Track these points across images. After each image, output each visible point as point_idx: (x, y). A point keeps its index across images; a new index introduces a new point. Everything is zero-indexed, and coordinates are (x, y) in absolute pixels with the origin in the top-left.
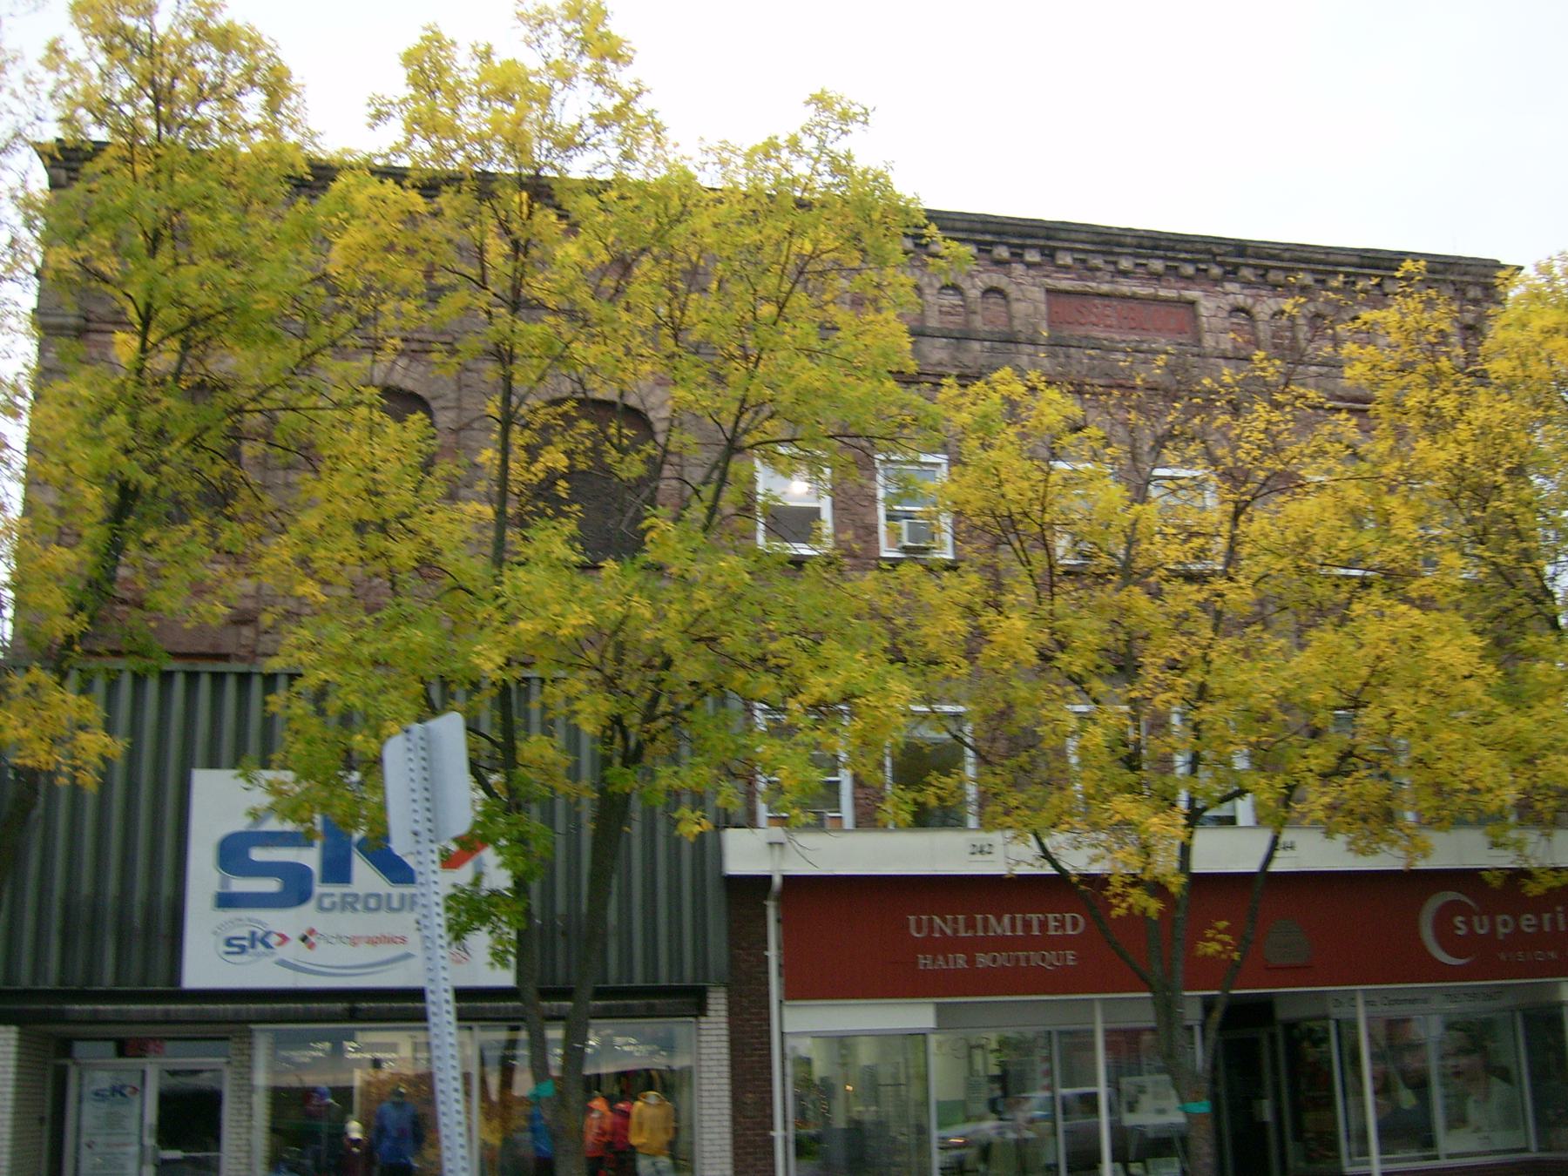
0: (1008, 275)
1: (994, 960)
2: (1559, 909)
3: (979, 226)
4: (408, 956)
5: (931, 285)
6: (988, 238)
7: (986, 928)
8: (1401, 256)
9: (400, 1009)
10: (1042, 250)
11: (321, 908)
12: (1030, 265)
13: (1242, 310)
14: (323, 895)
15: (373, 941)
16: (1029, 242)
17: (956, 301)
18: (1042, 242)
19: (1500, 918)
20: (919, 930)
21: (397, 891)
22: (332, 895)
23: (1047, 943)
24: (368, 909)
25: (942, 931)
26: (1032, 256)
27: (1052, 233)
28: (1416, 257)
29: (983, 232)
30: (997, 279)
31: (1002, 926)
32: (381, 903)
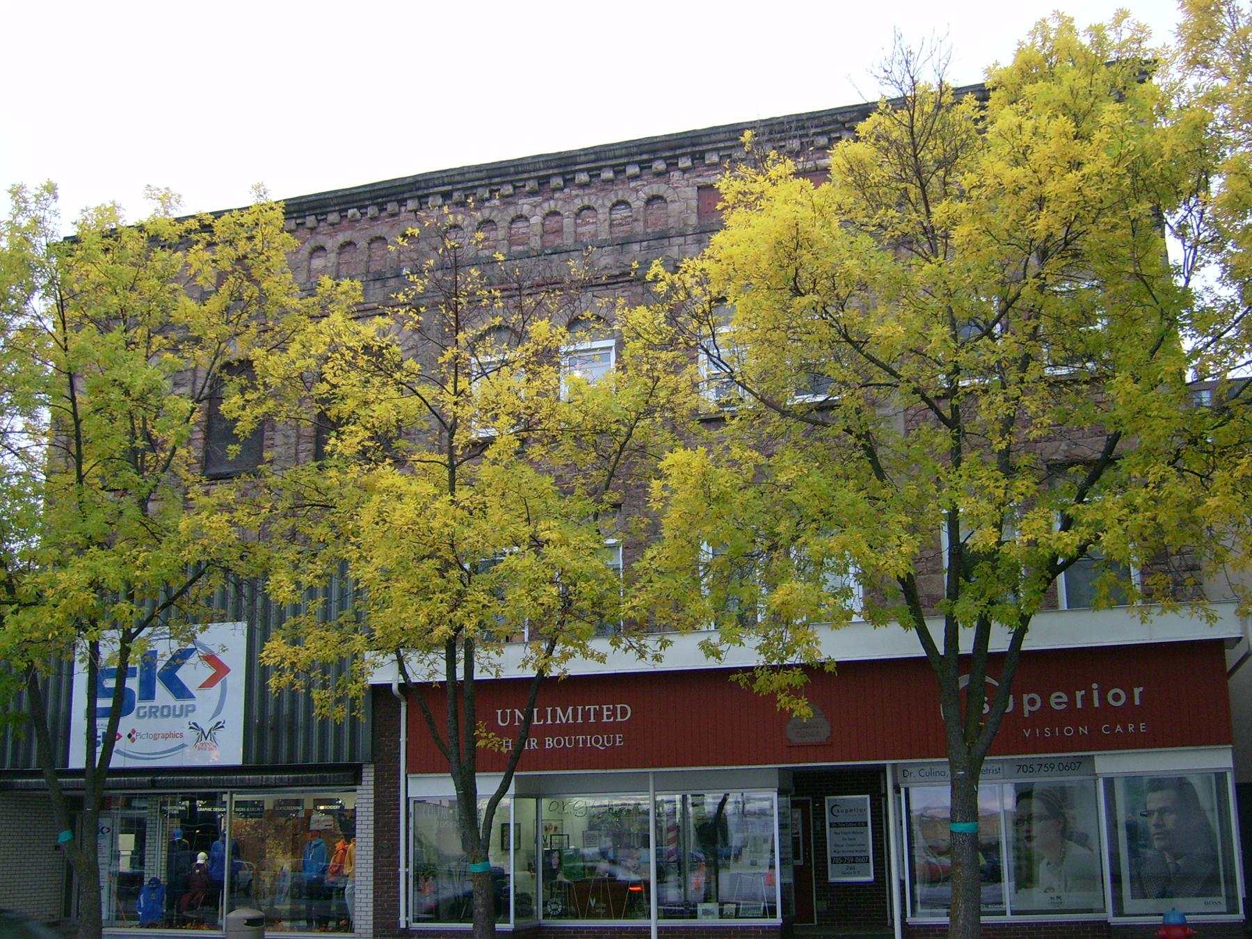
0: (667, 183)
1: (559, 742)
2: (1095, 686)
3: (635, 150)
4: (183, 746)
5: (603, 205)
6: (645, 157)
7: (554, 717)
8: (737, 130)
9: (178, 781)
10: (693, 156)
11: (139, 716)
12: (684, 171)
13: (581, 210)
14: (139, 708)
15: (165, 736)
16: (678, 152)
17: (626, 213)
18: (689, 150)
19: (1026, 697)
20: (504, 720)
21: (179, 703)
22: (145, 707)
23: (600, 728)
24: (163, 715)
25: (560, 720)
26: (685, 163)
27: (695, 141)
28: (752, 125)
29: (641, 154)
30: (657, 188)
31: (564, 716)
32: (166, 712)
